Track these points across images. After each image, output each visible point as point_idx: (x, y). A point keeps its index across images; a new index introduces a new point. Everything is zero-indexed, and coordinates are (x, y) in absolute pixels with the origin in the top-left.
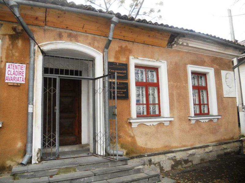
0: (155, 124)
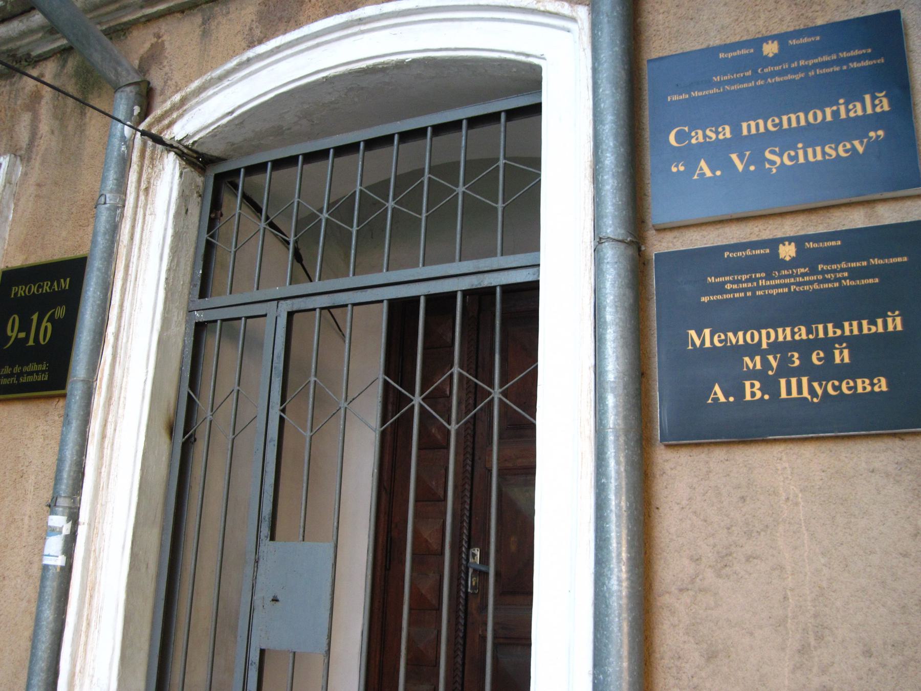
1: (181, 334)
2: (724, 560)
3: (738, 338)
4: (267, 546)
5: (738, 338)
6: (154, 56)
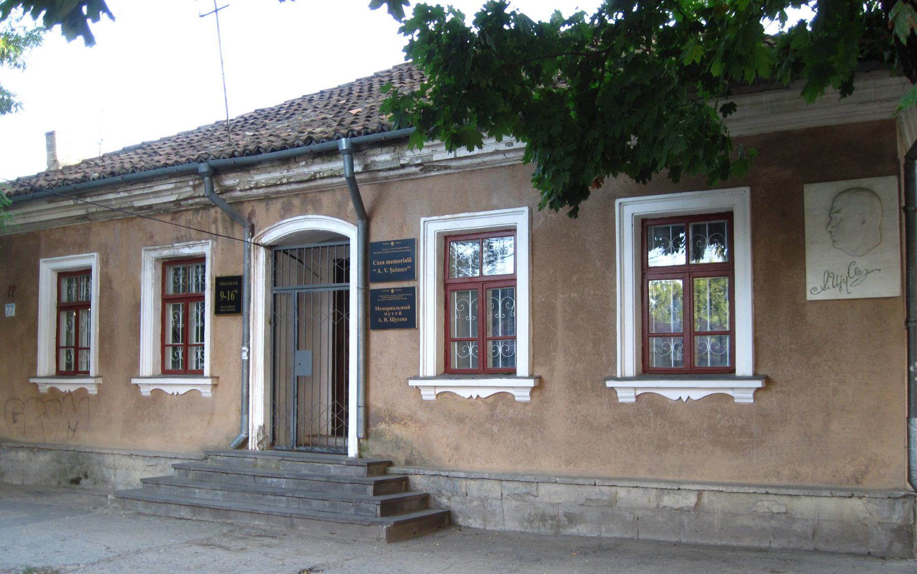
0: (484, 394)
1: (270, 296)
2: (381, 353)
3: (384, 309)
4: (297, 352)
5: (384, 309)
6: (252, 214)
